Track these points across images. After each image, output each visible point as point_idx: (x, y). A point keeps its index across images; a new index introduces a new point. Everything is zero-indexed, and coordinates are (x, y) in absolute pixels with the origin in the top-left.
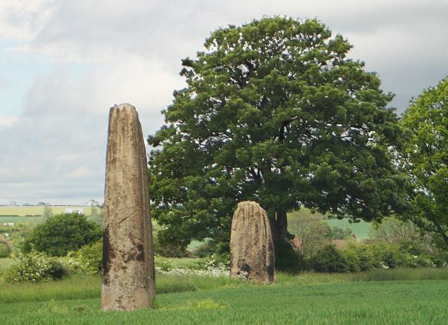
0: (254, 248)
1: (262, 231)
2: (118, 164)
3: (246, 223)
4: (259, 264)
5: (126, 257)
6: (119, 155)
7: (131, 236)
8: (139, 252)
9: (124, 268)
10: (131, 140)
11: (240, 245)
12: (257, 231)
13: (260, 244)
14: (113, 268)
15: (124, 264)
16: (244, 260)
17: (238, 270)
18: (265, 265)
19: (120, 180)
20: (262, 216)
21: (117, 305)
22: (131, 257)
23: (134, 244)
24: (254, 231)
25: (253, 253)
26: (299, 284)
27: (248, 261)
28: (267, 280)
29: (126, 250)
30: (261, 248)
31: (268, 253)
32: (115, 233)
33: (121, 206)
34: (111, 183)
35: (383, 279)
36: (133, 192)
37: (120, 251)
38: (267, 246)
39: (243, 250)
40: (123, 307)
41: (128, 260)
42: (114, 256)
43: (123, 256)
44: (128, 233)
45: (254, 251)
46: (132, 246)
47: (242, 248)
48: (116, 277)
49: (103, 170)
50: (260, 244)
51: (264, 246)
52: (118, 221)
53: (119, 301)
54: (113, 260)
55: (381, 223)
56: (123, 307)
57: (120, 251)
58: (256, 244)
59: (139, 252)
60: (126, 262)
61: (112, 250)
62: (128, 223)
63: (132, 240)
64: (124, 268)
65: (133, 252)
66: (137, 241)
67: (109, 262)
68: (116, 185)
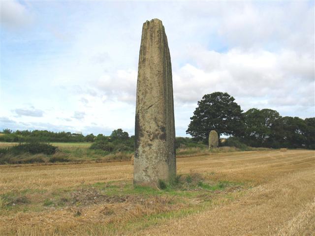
7: (155, 119)
15: (150, 142)
22: (155, 137)
27: (213, 144)
29: (152, 130)
45: (214, 142)
48: (144, 152)
54: (142, 139)
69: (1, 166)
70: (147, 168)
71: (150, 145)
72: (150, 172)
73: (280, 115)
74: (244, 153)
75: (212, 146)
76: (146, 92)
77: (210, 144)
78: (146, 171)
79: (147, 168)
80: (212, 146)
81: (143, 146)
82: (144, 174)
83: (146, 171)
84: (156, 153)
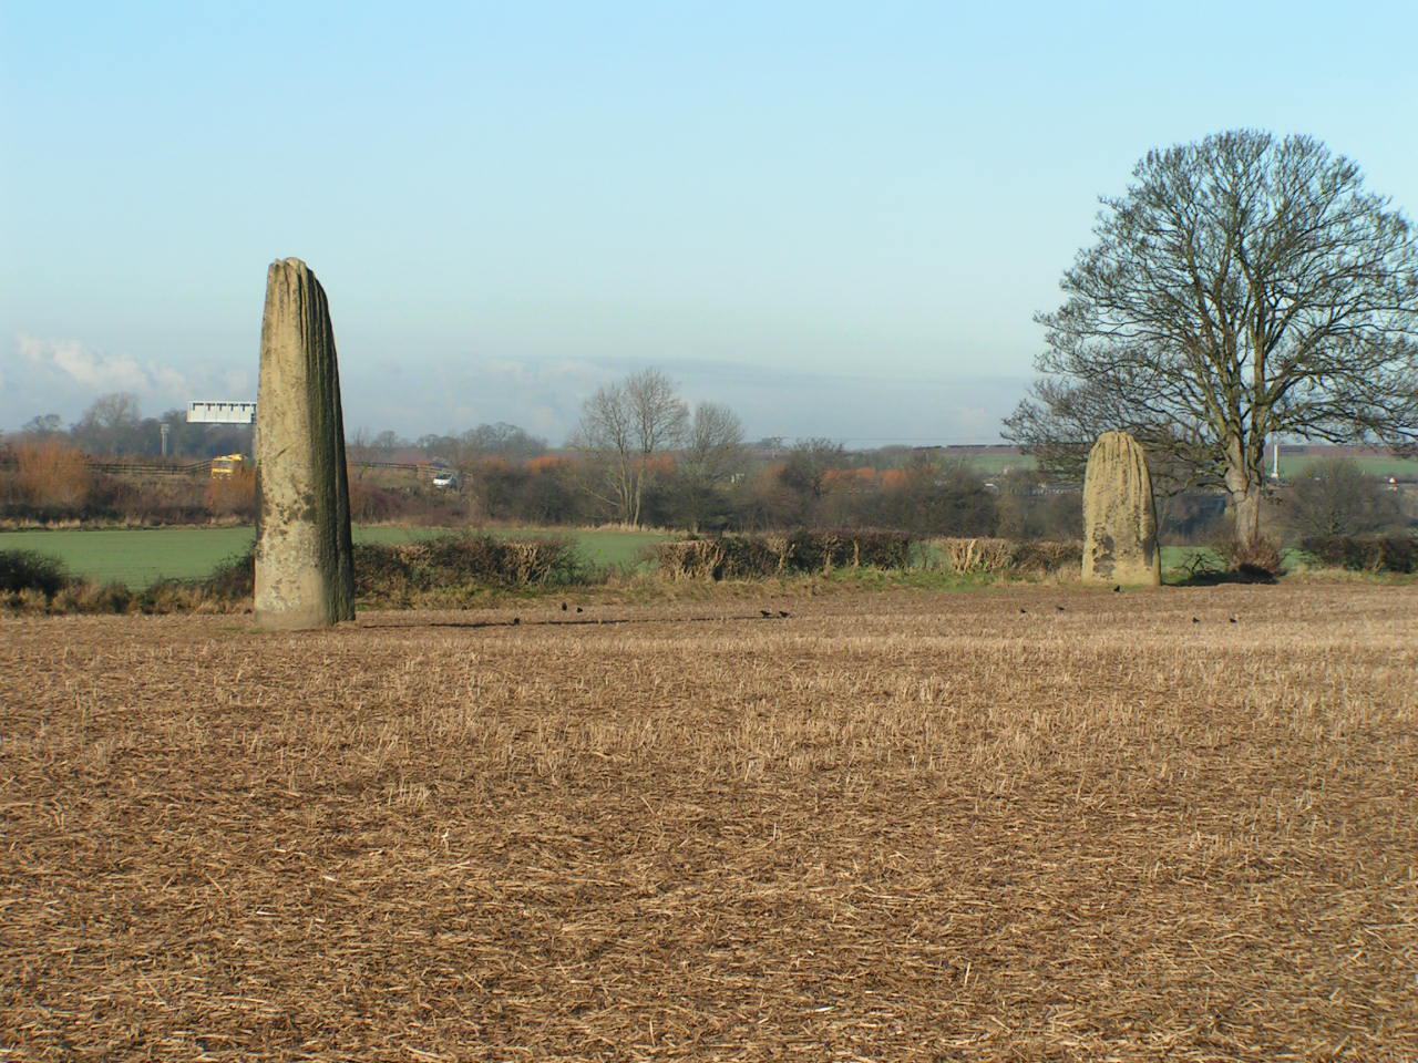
1: (1133, 482)
2: (274, 358)
3: (1109, 467)
4: (1129, 536)
5: (286, 514)
6: (274, 344)
8: (306, 507)
9: (284, 533)
11: (1098, 503)
12: (1125, 482)
14: (267, 532)
15: (283, 527)
16: (1104, 529)
17: (1095, 545)
18: (1138, 538)
19: (277, 385)
20: (1134, 457)
21: (274, 594)
22: (294, 515)
23: (299, 493)
24: (1119, 482)
25: (1118, 518)
27: (1110, 531)
28: (1142, 562)
29: (286, 502)
30: (1132, 509)
31: (1143, 517)
32: (270, 474)
33: (278, 429)
34: (264, 390)
35: (44, 519)
36: (295, 406)
37: (278, 505)
38: (1142, 507)
39: (1103, 513)
40: (282, 599)
41: (289, 519)
42: (269, 513)
43: (281, 513)
44: (288, 474)
45: (1122, 514)
46: (296, 497)
47: (1100, 509)
48: (272, 547)
49: (257, 360)
51: (1137, 507)
52: (273, 454)
53: (276, 588)
54: (268, 519)
56: (282, 599)
57: (278, 505)
58: (1123, 503)
59: (306, 507)
60: (285, 523)
61: (266, 502)
63: (295, 486)
64: (284, 533)
65: (296, 507)
66: (302, 488)
67: (263, 522)
68: (271, 393)
70: (279, 582)
77: (1089, 531)
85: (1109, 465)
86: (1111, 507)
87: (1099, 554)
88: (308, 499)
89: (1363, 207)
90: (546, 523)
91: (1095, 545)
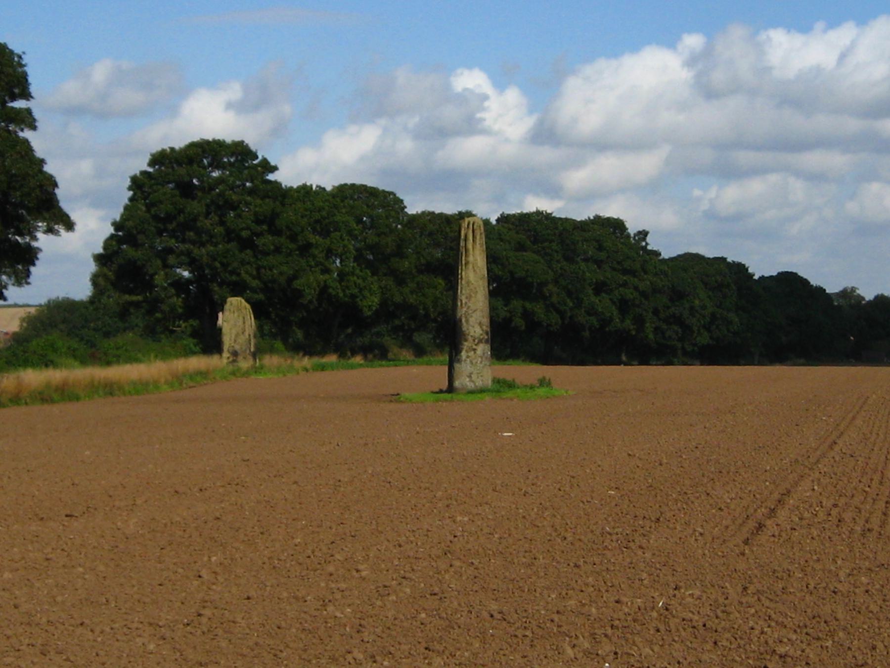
0: (242, 336)
1: (248, 323)
7: (480, 324)
10: (324, 289)
12: (244, 323)
13: (247, 334)
15: (474, 347)
17: (228, 355)
22: (480, 341)
26: (658, 631)
27: (237, 347)
29: (477, 335)
32: (467, 321)
39: (233, 338)
42: (466, 340)
45: (242, 339)
48: (468, 357)
50: (247, 334)
54: (466, 343)
55: (519, 243)
62: (478, 313)
64: (475, 350)
69: (9, 381)
70: (471, 373)
71: (475, 350)
72: (474, 377)
73: (295, 187)
74: (64, 393)
75: (235, 354)
76: (471, 296)
77: (226, 347)
78: (470, 376)
79: (471, 373)
80: (235, 354)
81: (467, 351)
82: (468, 379)
83: (470, 376)
84: (482, 357)
85: (236, 314)
86: (237, 335)
87: (231, 359)
88: (487, 333)
89: (635, 235)
90: (84, 362)
91: (228, 355)
